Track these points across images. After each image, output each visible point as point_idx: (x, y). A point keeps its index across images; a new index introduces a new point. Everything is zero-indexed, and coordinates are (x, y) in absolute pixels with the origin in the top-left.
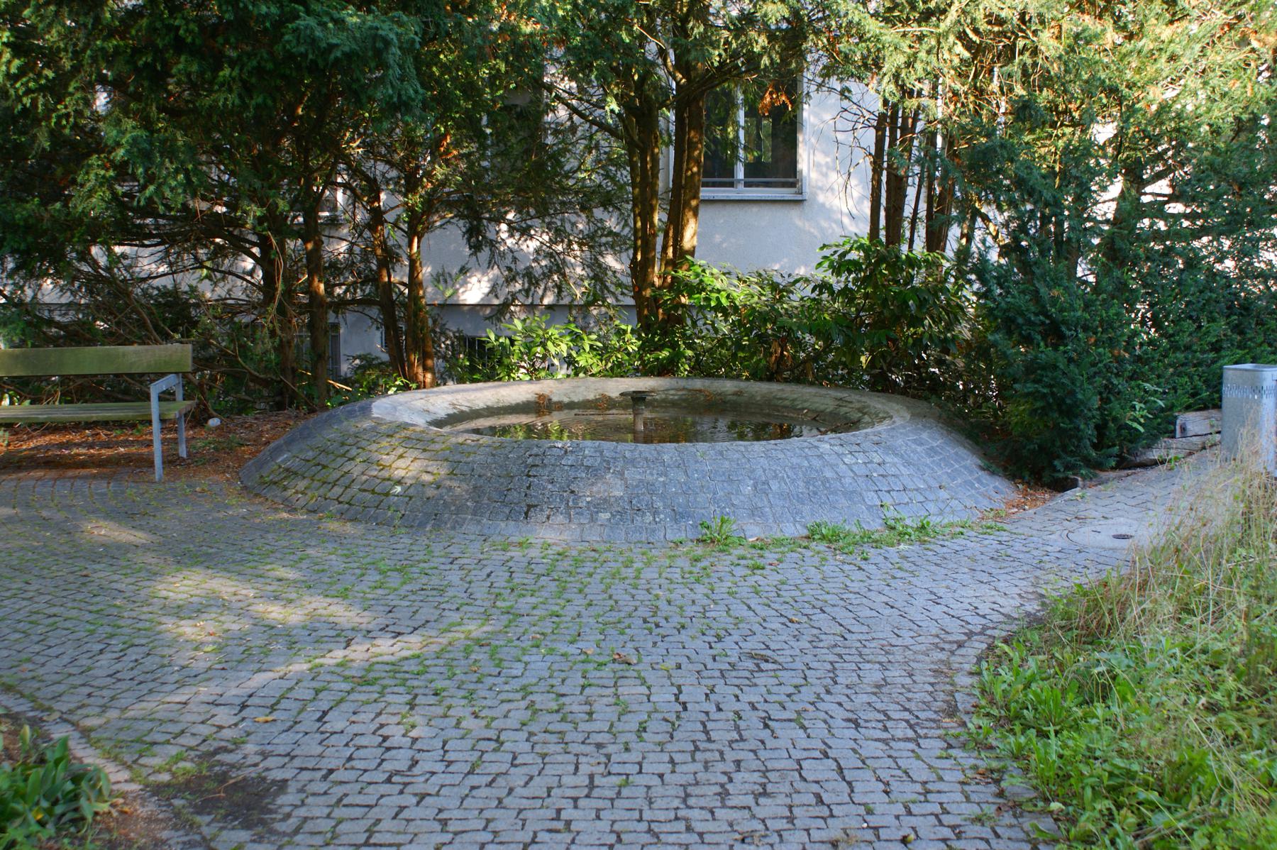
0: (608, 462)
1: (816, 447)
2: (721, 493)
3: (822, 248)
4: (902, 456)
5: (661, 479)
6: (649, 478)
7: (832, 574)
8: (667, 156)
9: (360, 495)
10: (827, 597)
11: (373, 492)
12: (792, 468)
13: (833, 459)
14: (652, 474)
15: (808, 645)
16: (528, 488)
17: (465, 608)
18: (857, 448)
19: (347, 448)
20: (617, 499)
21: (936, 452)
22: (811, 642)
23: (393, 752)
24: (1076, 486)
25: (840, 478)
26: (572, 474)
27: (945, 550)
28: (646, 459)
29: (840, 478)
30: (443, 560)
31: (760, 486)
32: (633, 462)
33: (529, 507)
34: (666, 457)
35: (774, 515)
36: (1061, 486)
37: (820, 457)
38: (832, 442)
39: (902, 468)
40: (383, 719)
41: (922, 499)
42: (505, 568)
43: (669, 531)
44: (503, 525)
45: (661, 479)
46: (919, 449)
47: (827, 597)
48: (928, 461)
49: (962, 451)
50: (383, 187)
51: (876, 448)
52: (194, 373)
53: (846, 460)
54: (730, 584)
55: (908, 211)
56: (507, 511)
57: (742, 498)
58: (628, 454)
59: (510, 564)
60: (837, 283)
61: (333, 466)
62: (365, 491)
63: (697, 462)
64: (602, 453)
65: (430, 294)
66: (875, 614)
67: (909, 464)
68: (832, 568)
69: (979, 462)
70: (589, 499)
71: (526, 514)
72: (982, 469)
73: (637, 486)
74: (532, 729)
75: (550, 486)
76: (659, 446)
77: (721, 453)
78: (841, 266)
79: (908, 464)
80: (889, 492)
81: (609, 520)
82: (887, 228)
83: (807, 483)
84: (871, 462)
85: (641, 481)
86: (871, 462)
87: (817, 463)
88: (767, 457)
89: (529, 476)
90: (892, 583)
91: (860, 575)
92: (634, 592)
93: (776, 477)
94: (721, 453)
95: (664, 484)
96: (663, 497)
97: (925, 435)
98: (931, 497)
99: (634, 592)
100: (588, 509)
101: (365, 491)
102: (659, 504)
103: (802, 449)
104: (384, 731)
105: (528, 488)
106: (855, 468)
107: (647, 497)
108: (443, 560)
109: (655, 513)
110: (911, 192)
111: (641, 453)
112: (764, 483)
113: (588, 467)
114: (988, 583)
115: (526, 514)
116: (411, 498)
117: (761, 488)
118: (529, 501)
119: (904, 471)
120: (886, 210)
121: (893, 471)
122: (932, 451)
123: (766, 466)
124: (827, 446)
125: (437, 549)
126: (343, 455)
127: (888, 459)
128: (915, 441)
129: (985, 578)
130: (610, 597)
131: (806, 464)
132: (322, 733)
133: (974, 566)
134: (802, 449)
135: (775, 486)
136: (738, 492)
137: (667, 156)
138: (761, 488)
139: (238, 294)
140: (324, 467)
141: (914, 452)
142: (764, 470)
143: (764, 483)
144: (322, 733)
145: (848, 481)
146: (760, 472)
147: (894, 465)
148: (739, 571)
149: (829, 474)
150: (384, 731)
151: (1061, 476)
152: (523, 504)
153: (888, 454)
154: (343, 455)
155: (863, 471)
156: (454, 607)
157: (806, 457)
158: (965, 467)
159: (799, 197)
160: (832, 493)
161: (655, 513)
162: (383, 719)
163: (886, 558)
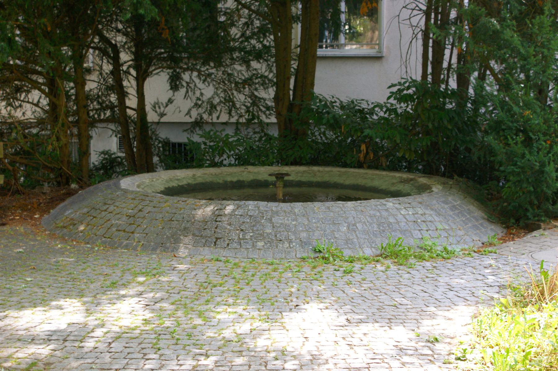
0: (263, 213)
1: (385, 205)
2: (328, 231)
3: (390, 87)
4: (436, 211)
5: (294, 223)
6: (287, 222)
7: (392, 276)
8: (297, 30)
9: (116, 233)
10: (388, 287)
11: (124, 231)
12: (370, 216)
13: (394, 212)
14: (288, 220)
15: (376, 311)
16: (216, 228)
17: (182, 293)
18: (408, 205)
19: (107, 206)
20: (268, 234)
21: (456, 208)
22: (378, 309)
23: (150, 361)
24: (540, 229)
25: (398, 223)
26: (242, 220)
27: (459, 263)
28: (285, 211)
29: (398, 223)
30: (168, 268)
31: (351, 227)
32: (277, 213)
33: (217, 239)
34: (296, 210)
35: (359, 243)
36: (530, 228)
37: (387, 210)
38: (394, 202)
39: (435, 217)
40: (143, 346)
41: (446, 235)
42: (204, 273)
43: (298, 252)
44: (201, 249)
45: (294, 223)
46: (446, 206)
47: (388, 287)
48: (451, 213)
49: (472, 208)
50: (121, 50)
51: (420, 205)
52: (160, 142)
53: (402, 212)
54: (332, 280)
55: (445, 65)
56: (204, 241)
57: (340, 233)
58: (274, 209)
59: (207, 270)
60: (401, 107)
61: (100, 216)
62: (119, 231)
63: (314, 213)
64: (259, 208)
65: (152, 117)
66: (416, 296)
67: (440, 215)
68: (392, 272)
69: (483, 214)
70: (251, 234)
71: (215, 243)
72: (484, 219)
73: (279, 227)
74: (225, 350)
75: (229, 227)
76: (293, 204)
77: (328, 208)
78: (401, 97)
79: (439, 215)
80: (427, 231)
81: (263, 246)
82: (432, 74)
83: (379, 225)
84: (417, 213)
85: (282, 224)
86: (417, 213)
87: (385, 214)
88: (356, 210)
89: (217, 221)
90: (426, 280)
91: (407, 276)
92: (279, 284)
93: (360, 222)
94: (328, 208)
95: (295, 225)
96: (295, 233)
97: (450, 199)
98: (452, 234)
99: (279, 284)
100: (251, 239)
101: (119, 231)
102: (293, 237)
103: (376, 206)
104: (144, 351)
105: (216, 228)
106: (407, 217)
107: (286, 233)
108: (168, 268)
109: (290, 242)
110: (447, 52)
111: (281, 208)
112: (353, 225)
113: (251, 216)
114: (482, 280)
115: (215, 243)
116: (147, 234)
117: (352, 227)
118: (216, 235)
119: (437, 219)
120: (432, 63)
121: (430, 218)
122: (453, 208)
123: (355, 216)
124: (391, 204)
125: (164, 262)
126: (105, 211)
127: (427, 212)
128: (443, 202)
129: (480, 278)
130: (265, 287)
131: (378, 214)
132: (110, 352)
133: (474, 271)
134: (376, 206)
135: (359, 226)
136: (339, 230)
137: (297, 30)
138: (352, 227)
139: (29, 114)
140: (95, 217)
141: (443, 208)
142: (354, 218)
143: (353, 225)
144: (110, 352)
145: (402, 224)
146: (351, 219)
147: (431, 215)
148: (338, 274)
149: (392, 220)
150: (144, 351)
151: (530, 222)
152: (213, 237)
153: (427, 209)
154: (105, 211)
155: (412, 218)
156: (177, 292)
157: (378, 211)
158: (474, 217)
159: (379, 55)
160: (394, 231)
161: (290, 242)
162: (143, 346)
163: (423, 267)
